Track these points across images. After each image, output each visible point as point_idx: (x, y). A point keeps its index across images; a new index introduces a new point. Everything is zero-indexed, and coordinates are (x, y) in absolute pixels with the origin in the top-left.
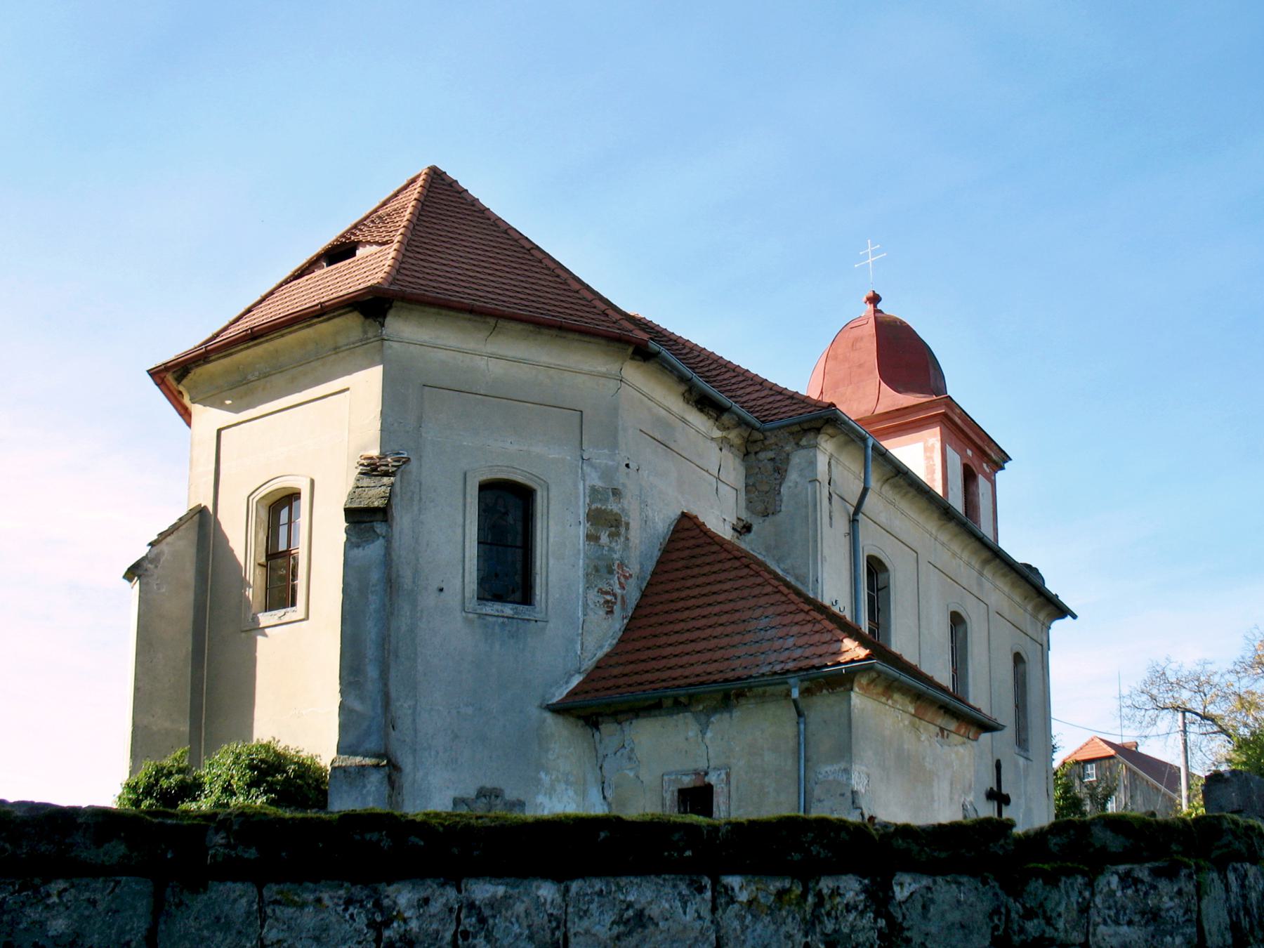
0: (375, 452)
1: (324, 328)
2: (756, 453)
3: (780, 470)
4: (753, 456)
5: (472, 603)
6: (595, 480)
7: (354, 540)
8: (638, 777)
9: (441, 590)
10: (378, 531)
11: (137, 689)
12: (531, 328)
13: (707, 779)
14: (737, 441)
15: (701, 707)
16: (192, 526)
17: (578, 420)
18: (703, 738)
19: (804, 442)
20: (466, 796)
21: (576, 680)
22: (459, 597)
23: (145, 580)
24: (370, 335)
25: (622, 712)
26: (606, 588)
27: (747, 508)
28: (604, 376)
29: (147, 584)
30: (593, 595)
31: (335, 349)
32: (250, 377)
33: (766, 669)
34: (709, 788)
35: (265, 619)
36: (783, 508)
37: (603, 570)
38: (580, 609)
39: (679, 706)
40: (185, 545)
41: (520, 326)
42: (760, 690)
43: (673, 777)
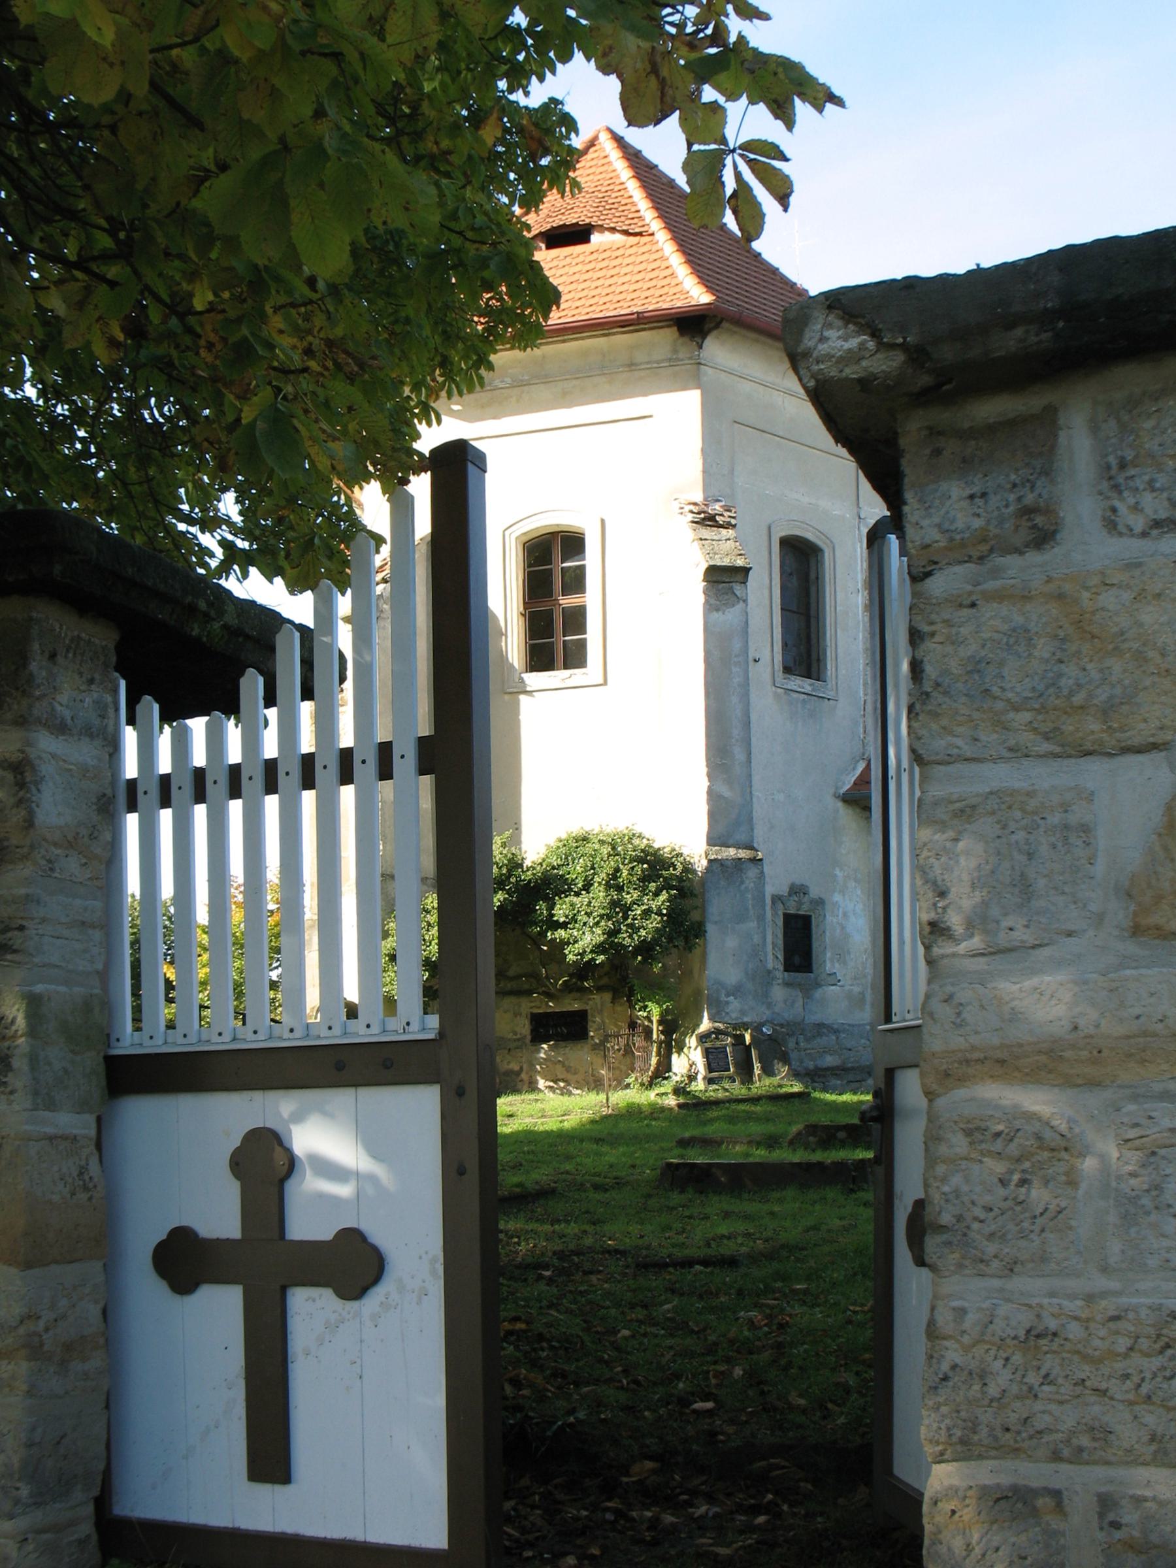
0: (699, 497)
1: (622, 340)
7: (713, 601)
10: (738, 593)
22: (769, 669)
24: (681, 355)
35: (534, 680)
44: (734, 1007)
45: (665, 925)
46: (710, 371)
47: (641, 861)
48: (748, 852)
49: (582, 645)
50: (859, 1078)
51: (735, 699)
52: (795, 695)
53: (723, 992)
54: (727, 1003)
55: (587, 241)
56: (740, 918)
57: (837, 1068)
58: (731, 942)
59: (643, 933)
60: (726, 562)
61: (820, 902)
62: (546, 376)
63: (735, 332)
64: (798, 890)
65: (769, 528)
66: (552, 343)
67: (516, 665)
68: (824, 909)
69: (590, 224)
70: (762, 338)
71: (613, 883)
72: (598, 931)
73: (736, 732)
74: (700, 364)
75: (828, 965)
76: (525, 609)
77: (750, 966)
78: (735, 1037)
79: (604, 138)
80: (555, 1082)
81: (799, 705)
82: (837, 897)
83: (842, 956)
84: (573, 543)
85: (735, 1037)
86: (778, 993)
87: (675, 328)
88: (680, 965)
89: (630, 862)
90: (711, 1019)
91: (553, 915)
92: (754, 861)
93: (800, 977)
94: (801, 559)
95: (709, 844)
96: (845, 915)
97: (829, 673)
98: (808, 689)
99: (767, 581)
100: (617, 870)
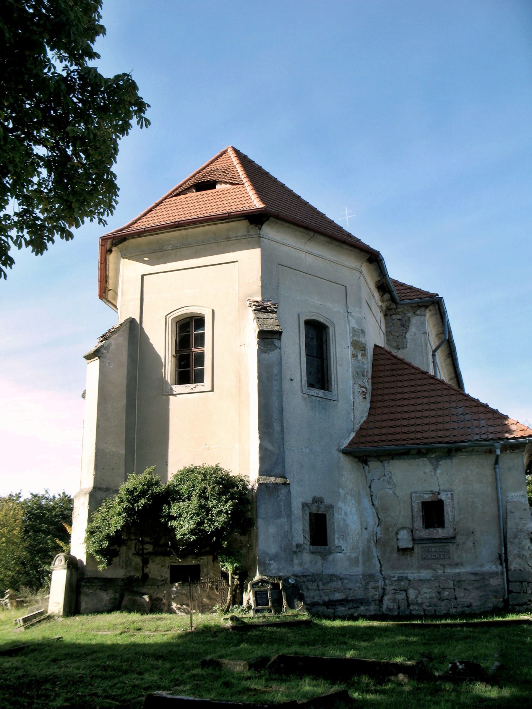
0: (259, 299)
1: (222, 226)
2: (391, 315)
3: (405, 325)
4: (389, 316)
5: (305, 388)
7: (262, 348)
10: (276, 344)
11: (98, 426)
12: (329, 240)
13: (439, 497)
14: (384, 308)
15: (433, 456)
16: (126, 329)
17: (344, 291)
18: (435, 473)
19: (418, 312)
20: (308, 502)
21: (353, 435)
23: (102, 360)
24: (251, 233)
25: (383, 455)
26: (363, 385)
29: (103, 362)
30: (358, 389)
32: (166, 248)
33: (477, 437)
34: (441, 503)
36: (408, 346)
37: (360, 374)
38: (352, 395)
40: (120, 342)
41: (324, 238)
42: (471, 449)
43: (418, 495)
44: (274, 567)
45: (230, 519)
46: (266, 240)
47: (219, 483)
48: (282, 479)
49: (202, 372)
50: (356, 606)
51: (275, 398)
52: (315, 398)
54: (270, 564)
55: (215, 188)
56: (278, 516)
57: (342, 600)
58: (272, 530)
59: (216, 524)
60: (269, 328)
61: (331, 507)
62: (188, 244)
63: (277, 223)
64: (317, 500)
65: (299, 315)
68: (333, 511)
69: (215, 180)
70: (291, 226)
71: (203, 495)
72: (192, 522)
73: (276, 415)
74: (260, 237)
75: (336, 541)
76: (176, 353)
78: (273, 584)
79: (231, 153)
80: (181, 605)
81: (317, 403)
82: (340, 504)
83: (344, 536)
84: (198, 321)
85: (273, 584)
86: (307, 557)
87: (247, 221)
88: (248, 541)
89: (213, 483)
90: (261, 573)
91: (170, 512)
92: (284, 484)
93: (320, 548)
94: (317, 333)
95: (260, 475)
97: (333, 387)
100: (205, 488)
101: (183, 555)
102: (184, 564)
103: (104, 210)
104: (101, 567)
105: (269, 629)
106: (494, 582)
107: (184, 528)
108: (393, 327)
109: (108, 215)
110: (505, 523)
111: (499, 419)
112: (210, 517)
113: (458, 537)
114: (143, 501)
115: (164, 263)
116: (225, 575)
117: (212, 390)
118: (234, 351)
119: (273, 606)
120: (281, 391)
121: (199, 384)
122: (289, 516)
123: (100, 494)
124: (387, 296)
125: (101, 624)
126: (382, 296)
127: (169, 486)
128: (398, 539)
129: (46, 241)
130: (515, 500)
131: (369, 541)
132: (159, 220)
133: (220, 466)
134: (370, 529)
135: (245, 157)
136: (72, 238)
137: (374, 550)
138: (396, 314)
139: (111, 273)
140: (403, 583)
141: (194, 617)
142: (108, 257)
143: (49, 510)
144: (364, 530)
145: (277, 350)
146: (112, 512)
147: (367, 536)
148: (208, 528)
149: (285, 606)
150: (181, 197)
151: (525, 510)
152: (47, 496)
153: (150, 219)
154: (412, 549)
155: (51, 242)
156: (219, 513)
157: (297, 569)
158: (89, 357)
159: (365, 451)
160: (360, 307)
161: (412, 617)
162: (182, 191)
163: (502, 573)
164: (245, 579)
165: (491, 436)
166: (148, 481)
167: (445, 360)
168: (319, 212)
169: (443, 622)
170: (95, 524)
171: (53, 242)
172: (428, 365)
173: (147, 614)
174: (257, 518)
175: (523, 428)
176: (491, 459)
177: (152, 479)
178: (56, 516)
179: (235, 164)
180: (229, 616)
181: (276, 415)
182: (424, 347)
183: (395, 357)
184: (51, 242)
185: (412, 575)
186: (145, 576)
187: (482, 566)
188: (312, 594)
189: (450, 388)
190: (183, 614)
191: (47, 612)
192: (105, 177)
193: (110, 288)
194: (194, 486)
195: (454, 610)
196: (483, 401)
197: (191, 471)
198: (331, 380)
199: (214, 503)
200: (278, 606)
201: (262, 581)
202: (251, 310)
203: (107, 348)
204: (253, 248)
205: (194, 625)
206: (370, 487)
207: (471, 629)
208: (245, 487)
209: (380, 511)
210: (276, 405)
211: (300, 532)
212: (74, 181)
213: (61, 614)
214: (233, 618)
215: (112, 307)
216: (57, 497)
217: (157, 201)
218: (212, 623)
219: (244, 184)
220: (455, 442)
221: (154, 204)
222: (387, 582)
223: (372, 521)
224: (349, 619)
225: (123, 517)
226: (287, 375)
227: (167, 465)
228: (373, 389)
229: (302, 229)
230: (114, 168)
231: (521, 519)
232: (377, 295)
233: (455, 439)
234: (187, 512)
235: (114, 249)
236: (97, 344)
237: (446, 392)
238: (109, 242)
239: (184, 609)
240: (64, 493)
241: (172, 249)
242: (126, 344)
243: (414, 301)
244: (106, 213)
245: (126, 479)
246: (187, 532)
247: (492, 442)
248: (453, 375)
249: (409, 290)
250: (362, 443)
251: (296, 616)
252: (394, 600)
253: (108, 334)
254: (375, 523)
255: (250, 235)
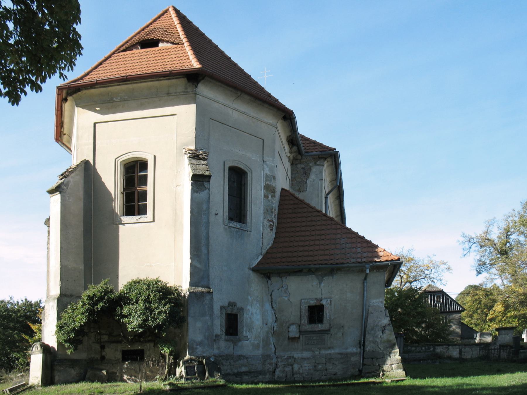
0: (193, 147)
1: (165, 83)
2: (296, 164)
3: (307, 173)
5: (226, 221)
6: (267, 171)
7: (195, 189)
8: (289, 300)
9: (216, 214)
10: (206, 186)
11: (61, 248)
13: (321, 302)
14: (292, 158)
15: (320, 273)
16: (81, 170)
19: (318, 163)
21: (260, 258)
22: (222, 218)
23: (63, 194)
26: (271, 219)
27: (291, 187)
28: (271, 125)
30: (266, 223)
31: (168, 94)
32: (115, 99)
33: (354, 260)
35: (125, 219)
36: (308, 190)
39: (310, 271)
40: (77, 179)
44: (199, 350)
46: (200, 97)
47: (159, 291)
49: (145, 206)
53: (195, 344)
54: (197, 348)
55: (158, 46)
57: (247, 372)
58: (199, 324)
59: (158, 320)
60: (201, 173)
61: (242, 309)
64: (232, 304)
66: (136, 83)
67: (119, 213)
68: (243, 312)
71: (147, 300)
72: (139, 319)
73: (203, 242)
74: (196, 94)
75: (244, 333)
77: (207, 334)
79: (172, 12)
80: (131, 377)
82: (249, 307)
83: (250, 328)
84: (143, 165)
85: (199, 362)
86: (222, 344)
87: (186, 79)
92: (209, 293)
93: (232, 337)
94: (238, 177)
96: (252, 314)
98: (239, 226)
99: (222, 183)
100: (149, 295)
101: (132, 342)
102: (132, 349)
103: (65, 66)
104: (69, 352)
105: (196, 390)
106: (353, 359)
107: (134, 323)
108: (297, 175)
109: (68, 70)
110: (366, 320)
111: (371, 247)
112: (153, 315)
113: (332, 330)
114: (101, 305)
115: (114, 113)
116: (163, 356)
117: (154, 221)
118: (172, 189)
119: (199, 376)
120: (208, 222)
121: (142, 216)
122: (211, 315)
123: (65, 299)
124: (295, 148)
125: (73, 390)
126: (291, 148)
127: (120, 294)
128: (289, 331)
129: (19, 93)
130: (375, 304)
131: (268, 333)
132: (109, 74)
133: (160, 279)
134: (269, 324)
135: (185, 17)
136: (41, 90)
137: (271, 339)
138: (300, 163)
139: (66, 120)
140: (290, 360)
141: (142, 384)
142: (63, 105)
143: (15, 312)
144: (264, 325)
145: (207, 191)
146: (76, 312)
147: (266, 329)
148: (152, 323)
149: (207, 376)
150: (128, 52)
151: (381, 311)
152: (12, 301)
153: (101, 72)
154: (299, 338)
155: (23, 94)
156: (160, 313)
157: (216, 352)
158: (52, 192)
159: (270, 269)
160: (273, 157)
161: (295, 382)
162: (129, 47)
163: (360, 353)
164: (178, 358)
165: (364, 260)
166: (105, 290)
167: (334, 202)
168: (245, 74)
169: (317, 384)
170: (63, 321)
171: (26, 94)
172: (321, 206)
173: (106, 383)
174: (187, 317)
175: (388, 254)
176: (362, 276)
177: (108, 288)
178: (21, 316)
179: (176, 24)
180: (167, 382)
181: (203, 242)
182: (320, 191)
183: (297, 198)
184: (23, 94)
185: (297, 355)
186: (103, 358)
187: (347, 348)
188: (226, 368)
189: (337, 223)
190: (132, 382)
191: (28, 384)
192: (71, 36)
193: (65, 133)
194: (140, 294)
195: (325, 377)
196: (361, 234)
197: (138, 282)
198: (247, 215)
199: (156, 305)
200: (202, 375)
201: (191, 359)
202: (186, 157)
203: (67, 185)
204: (189, 103)
205: (142, 389)
206: (271, 295)
207: (336, 388)
208: (179, 294)
209: (277, 312)
210: (204, 234)
211: (218, 326)
212: (42, 38)
213: (40, 384)
214: (170, 384)
215: (67, 149)
216: (21, 302)
217: (107, 55)
218: (155, 387)
219: (183, 44)
220: (337, 264)
221: (103, 58)
222: (279, 360)
223: (270, 318)
224: (252, 384)
225: (86, 316)
226: (213, 211)
227: (118, 278)
228: (278, 223)
229: (231, 89)
230: (79, 28)
231: (377, 318)
232: (287, 147)
233: (338, 261)
234: (136, 313)
235: (69, 98)
236: (58, 181)
237: (334, 227)
238: (65, 92)
239: (133, 379)
240: (26, 299)
241: (120, 101)
242: (82, 182)
243: (317, 153)
244: (67, 68)
245: (86, 288)
246: (135, 326)
247: (364, 264)
248: (339, 213)
249: (312, 144)
250: (268, 263)
251: (216, 382)
252: (283, 371)
253: (67, 173)
254: (273, 321)
255: (187, 92)
